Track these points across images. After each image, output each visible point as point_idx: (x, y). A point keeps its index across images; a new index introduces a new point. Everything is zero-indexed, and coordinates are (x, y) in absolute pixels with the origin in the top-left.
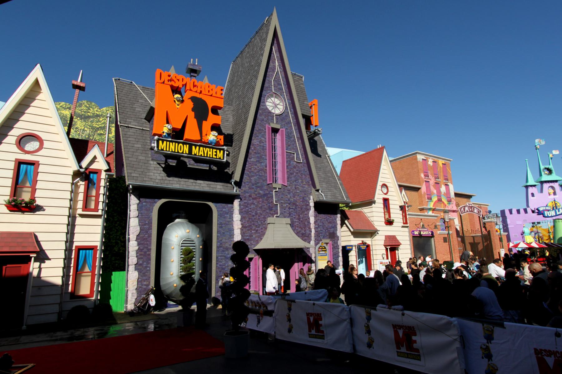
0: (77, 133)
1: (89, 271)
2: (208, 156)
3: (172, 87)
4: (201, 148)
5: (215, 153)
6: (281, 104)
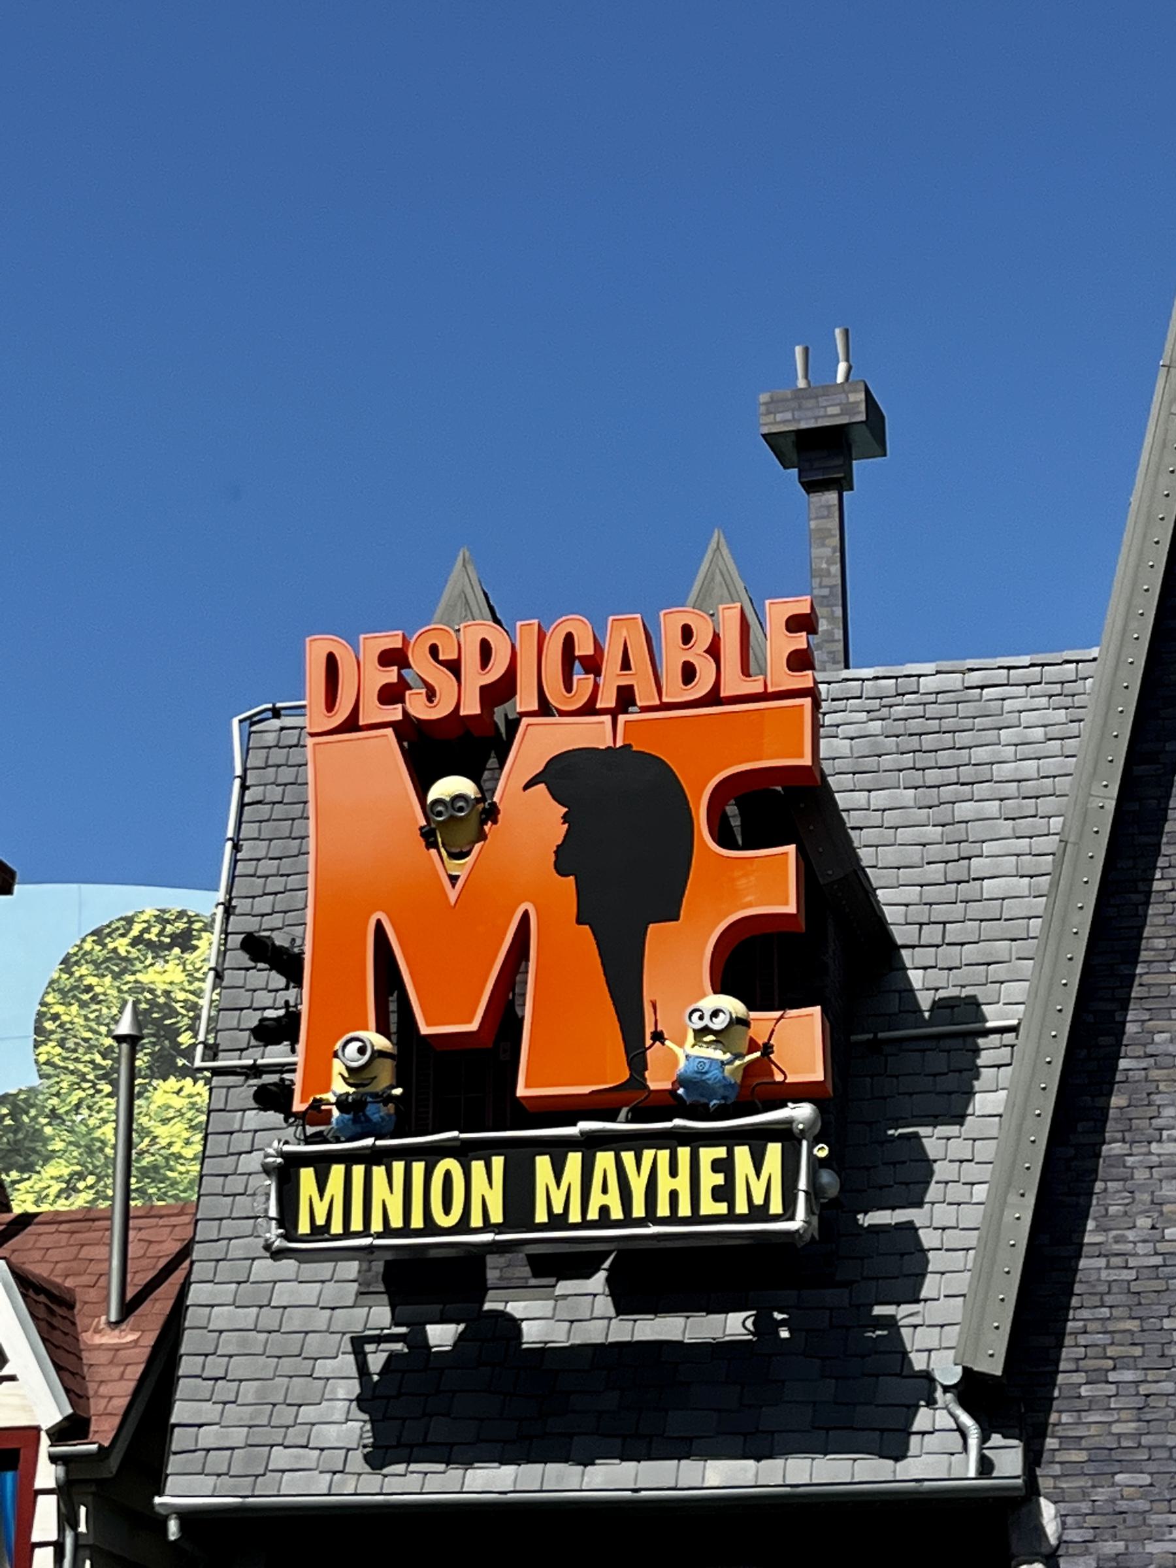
2: (663, 1210)
4: (604, 1160)
5: (720, 1179)
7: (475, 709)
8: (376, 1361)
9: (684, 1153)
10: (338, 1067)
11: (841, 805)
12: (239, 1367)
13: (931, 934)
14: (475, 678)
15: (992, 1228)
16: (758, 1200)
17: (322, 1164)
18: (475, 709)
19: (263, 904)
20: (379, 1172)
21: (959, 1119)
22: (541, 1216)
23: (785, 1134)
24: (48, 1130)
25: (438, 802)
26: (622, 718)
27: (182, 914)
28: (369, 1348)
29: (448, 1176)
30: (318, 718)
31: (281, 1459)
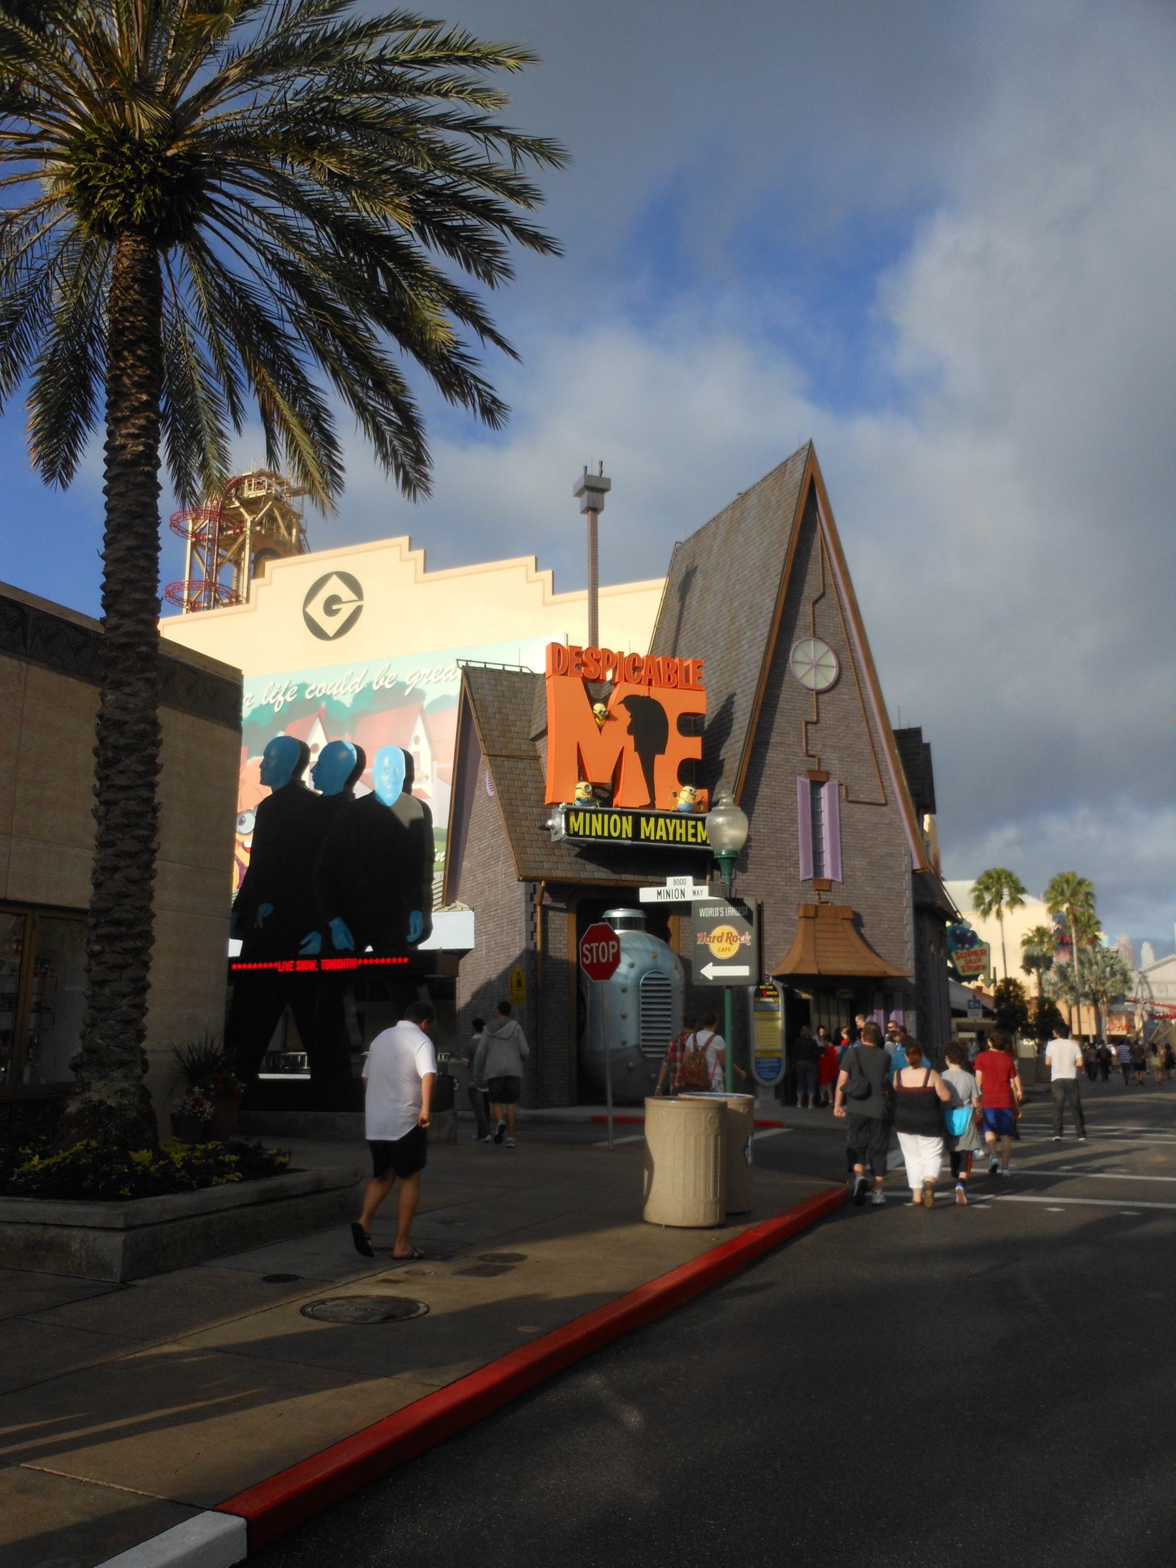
5: (693, 831)
16: (648, 835)
17: (648, 817)
22: (643, 836)
29: (615, 820)
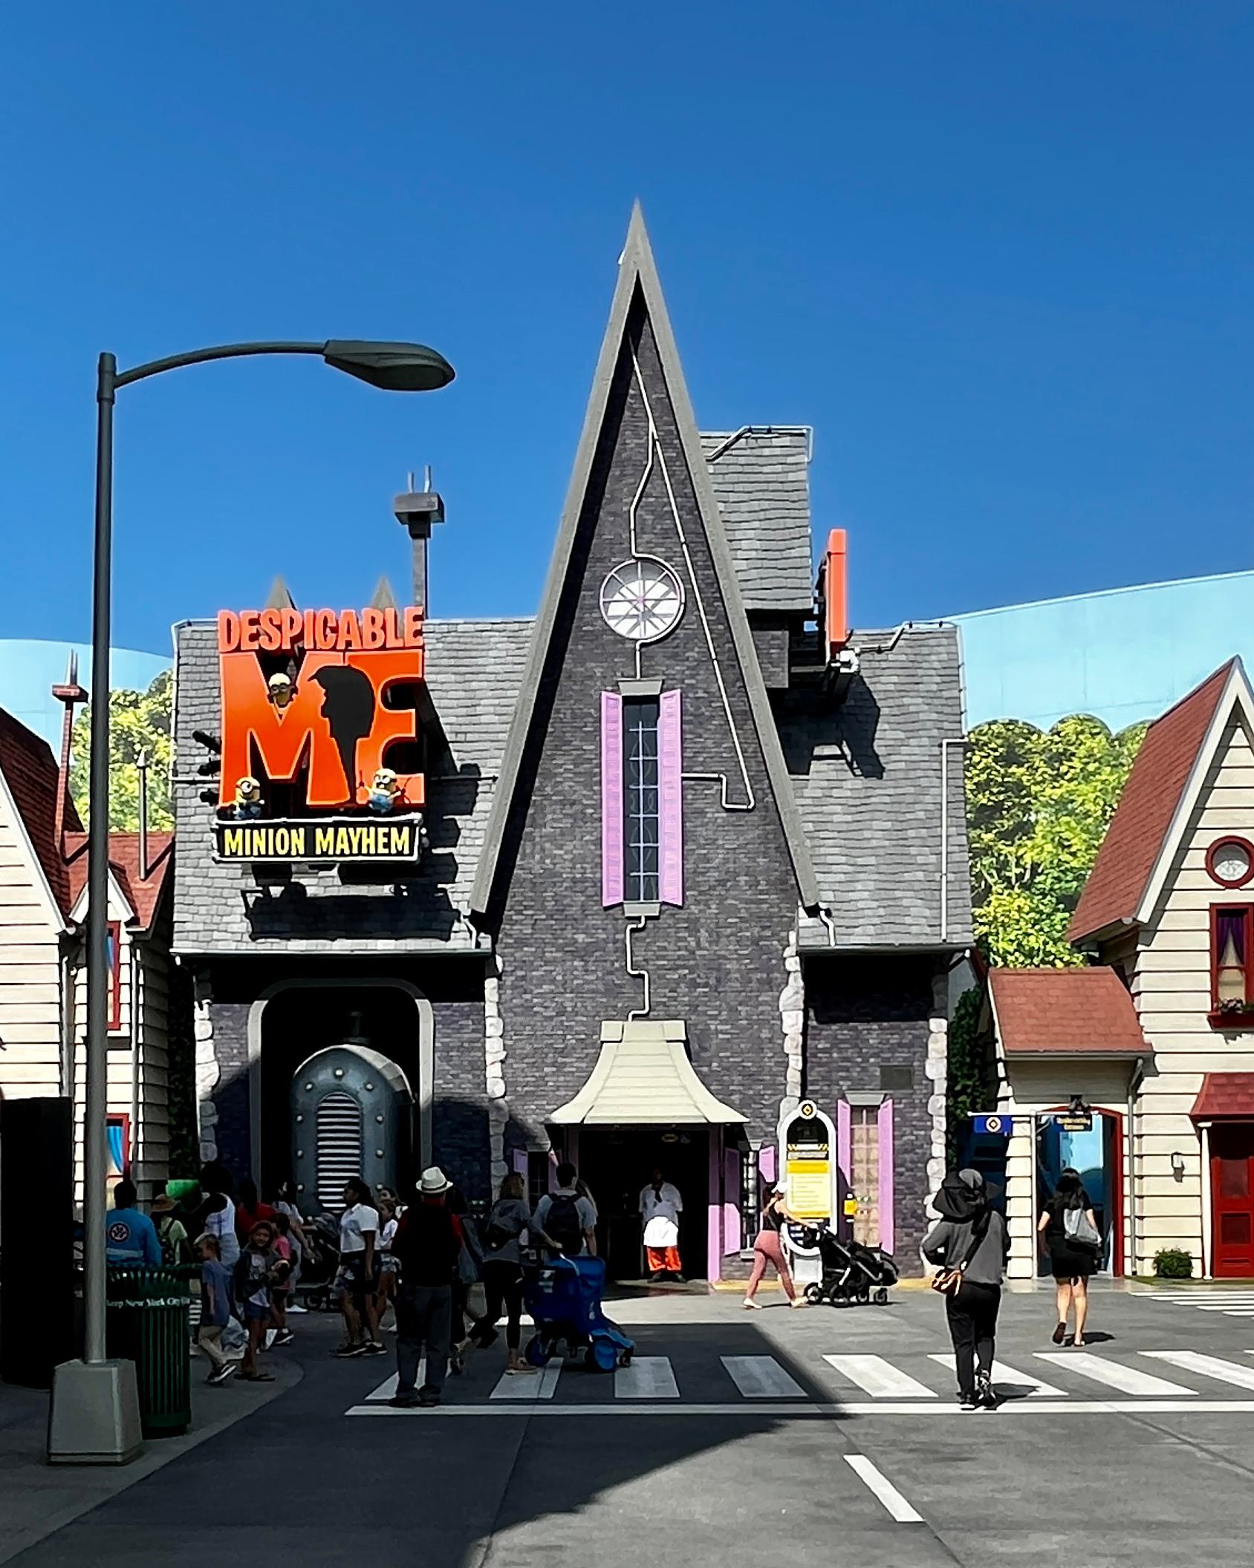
0: (161, 778)
1: (119, 1173)
2: (364, 851)
3: (262, 654)
4: (342, 831)
5: (386, 840)
6: (672, 595)
7: (288, 647)
8: (251, 900)
9: (372, 829)
10: (238, 792)
11: (429, 688)
12: (197, 901)
13: (461, 737)
14: (289, 634)
15: (484, 857)
18: (288, 647)
19: (191, 710)
20: (256, 832)
21: (471, 813)
22: (318, 852)
23: (410, 824)
24: (80, 784)
25: (274, 686)
26: (347, 654)
27: (133, 692)
28: (248, 895)
30: (223, 646)
31: (216, 935)
